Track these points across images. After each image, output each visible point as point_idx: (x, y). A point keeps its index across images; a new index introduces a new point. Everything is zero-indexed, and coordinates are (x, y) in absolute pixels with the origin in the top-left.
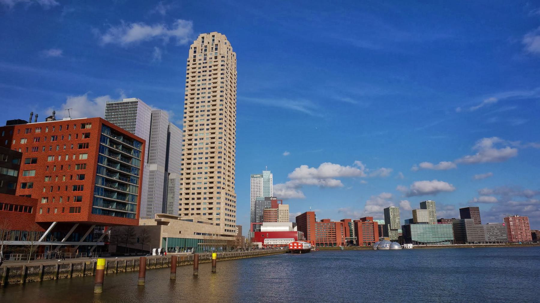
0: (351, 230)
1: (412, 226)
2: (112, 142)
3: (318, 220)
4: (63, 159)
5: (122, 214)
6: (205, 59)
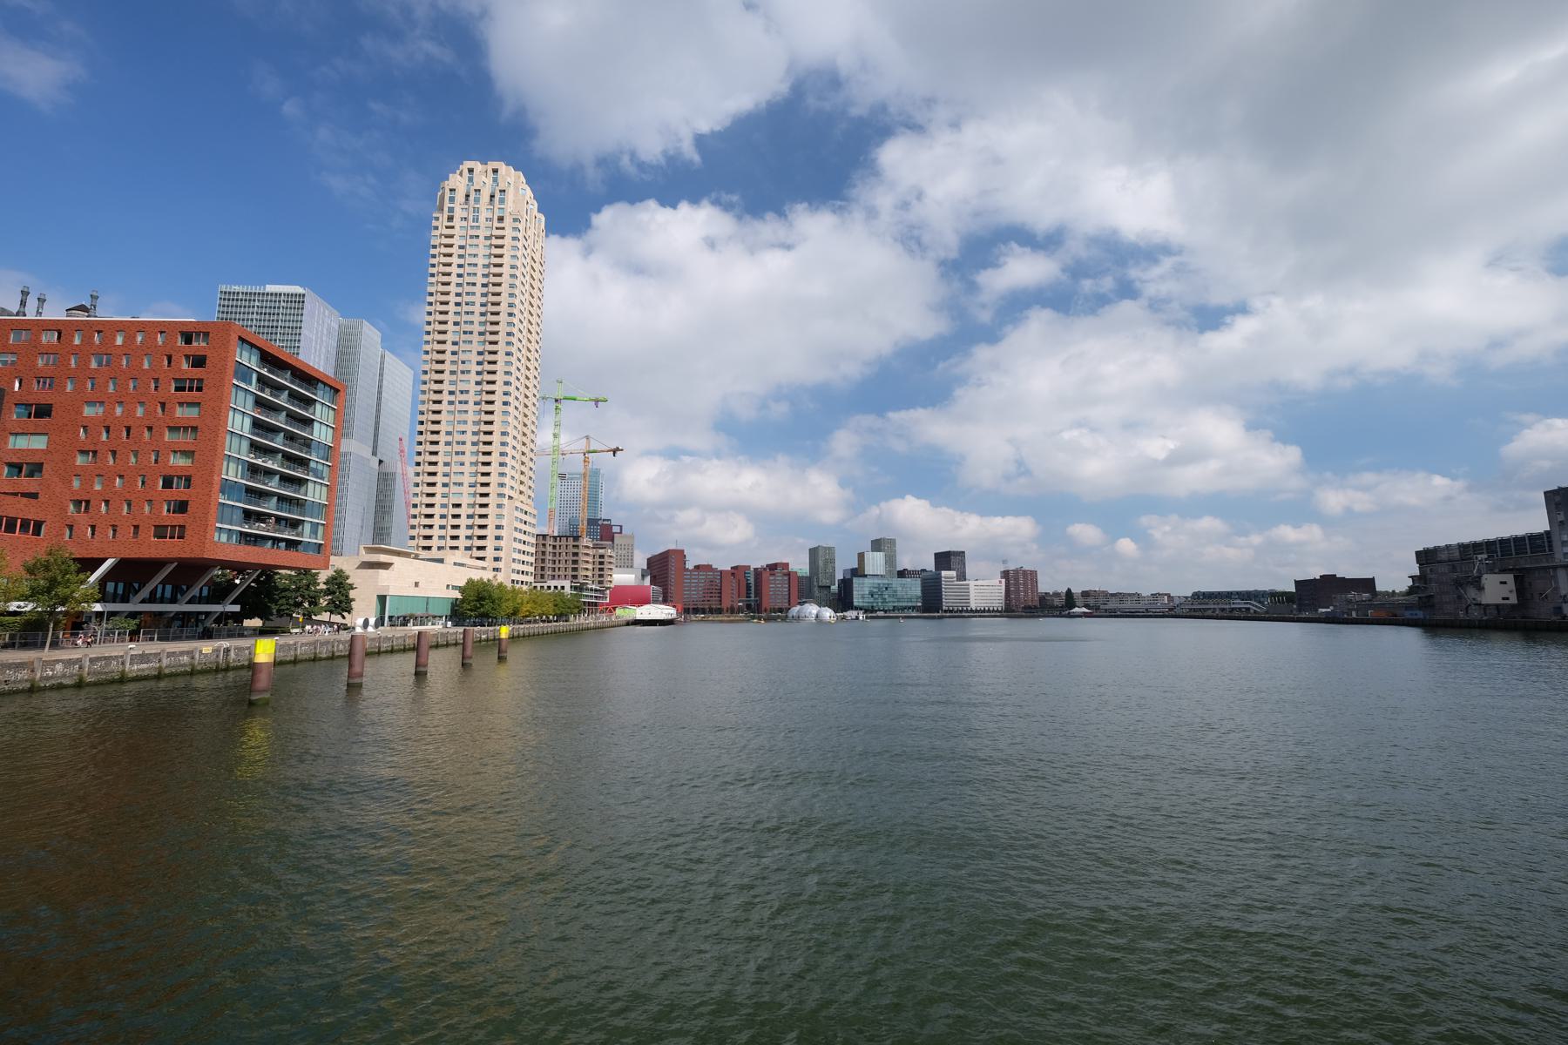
0: (748, 587)
1: (855, 580)
2: (262, 381)
3: (690, 566)
4: (130, 413)
5: (292, 544)
6: (476, 219)
